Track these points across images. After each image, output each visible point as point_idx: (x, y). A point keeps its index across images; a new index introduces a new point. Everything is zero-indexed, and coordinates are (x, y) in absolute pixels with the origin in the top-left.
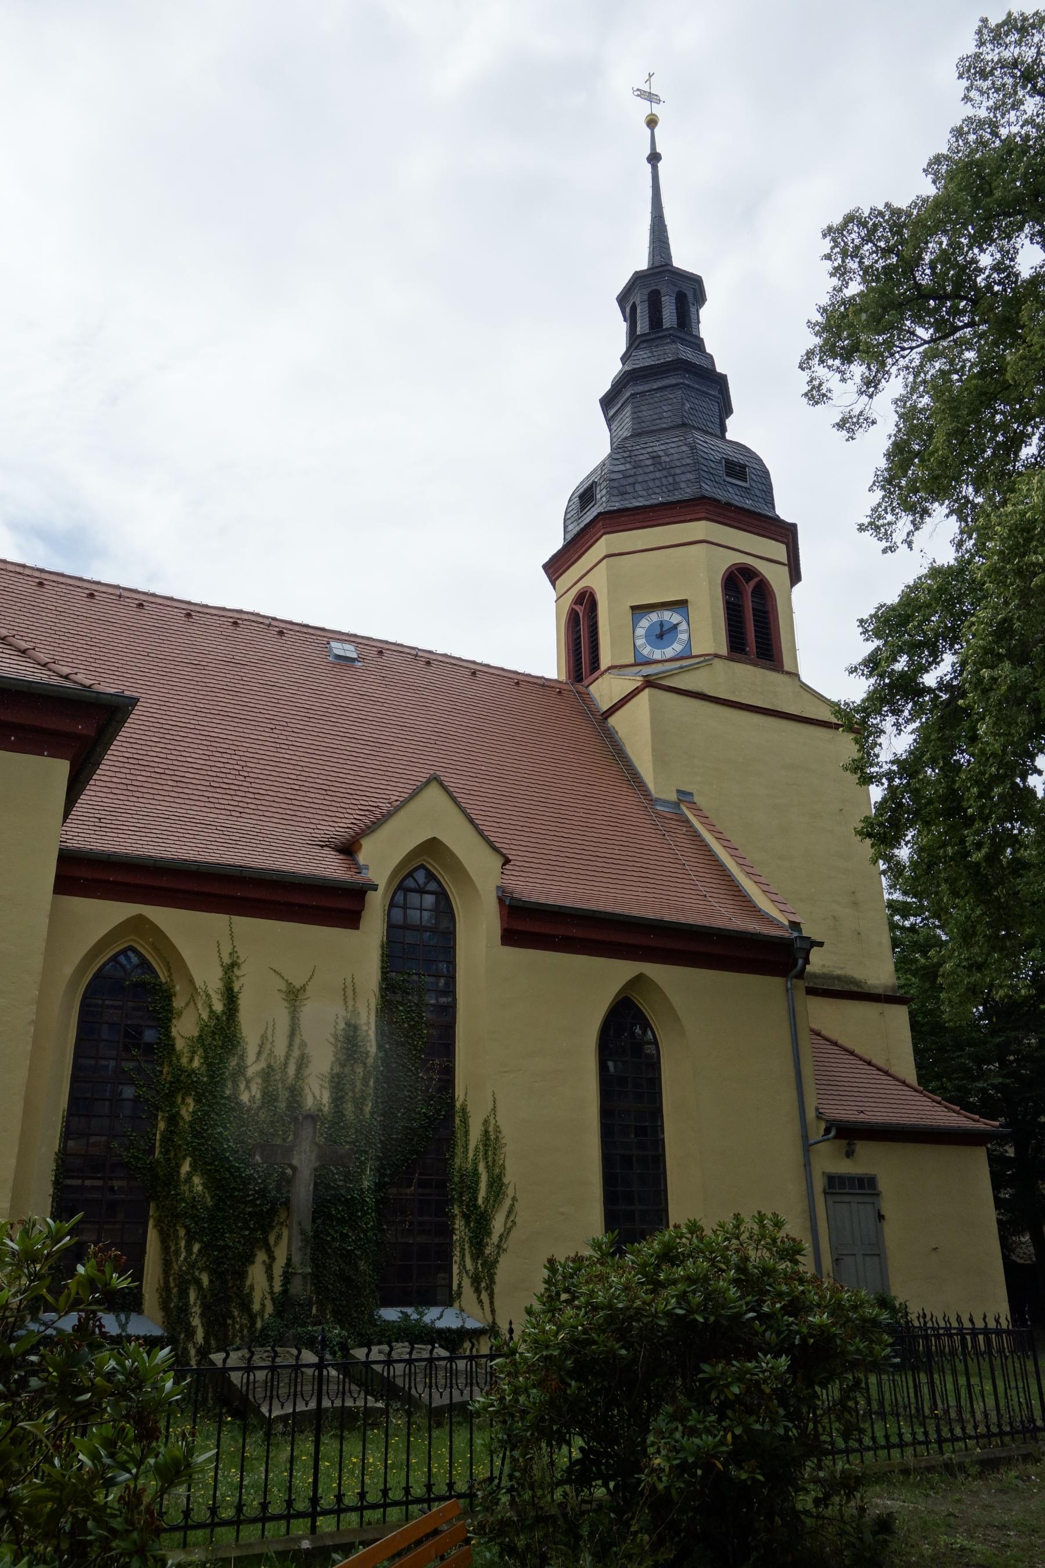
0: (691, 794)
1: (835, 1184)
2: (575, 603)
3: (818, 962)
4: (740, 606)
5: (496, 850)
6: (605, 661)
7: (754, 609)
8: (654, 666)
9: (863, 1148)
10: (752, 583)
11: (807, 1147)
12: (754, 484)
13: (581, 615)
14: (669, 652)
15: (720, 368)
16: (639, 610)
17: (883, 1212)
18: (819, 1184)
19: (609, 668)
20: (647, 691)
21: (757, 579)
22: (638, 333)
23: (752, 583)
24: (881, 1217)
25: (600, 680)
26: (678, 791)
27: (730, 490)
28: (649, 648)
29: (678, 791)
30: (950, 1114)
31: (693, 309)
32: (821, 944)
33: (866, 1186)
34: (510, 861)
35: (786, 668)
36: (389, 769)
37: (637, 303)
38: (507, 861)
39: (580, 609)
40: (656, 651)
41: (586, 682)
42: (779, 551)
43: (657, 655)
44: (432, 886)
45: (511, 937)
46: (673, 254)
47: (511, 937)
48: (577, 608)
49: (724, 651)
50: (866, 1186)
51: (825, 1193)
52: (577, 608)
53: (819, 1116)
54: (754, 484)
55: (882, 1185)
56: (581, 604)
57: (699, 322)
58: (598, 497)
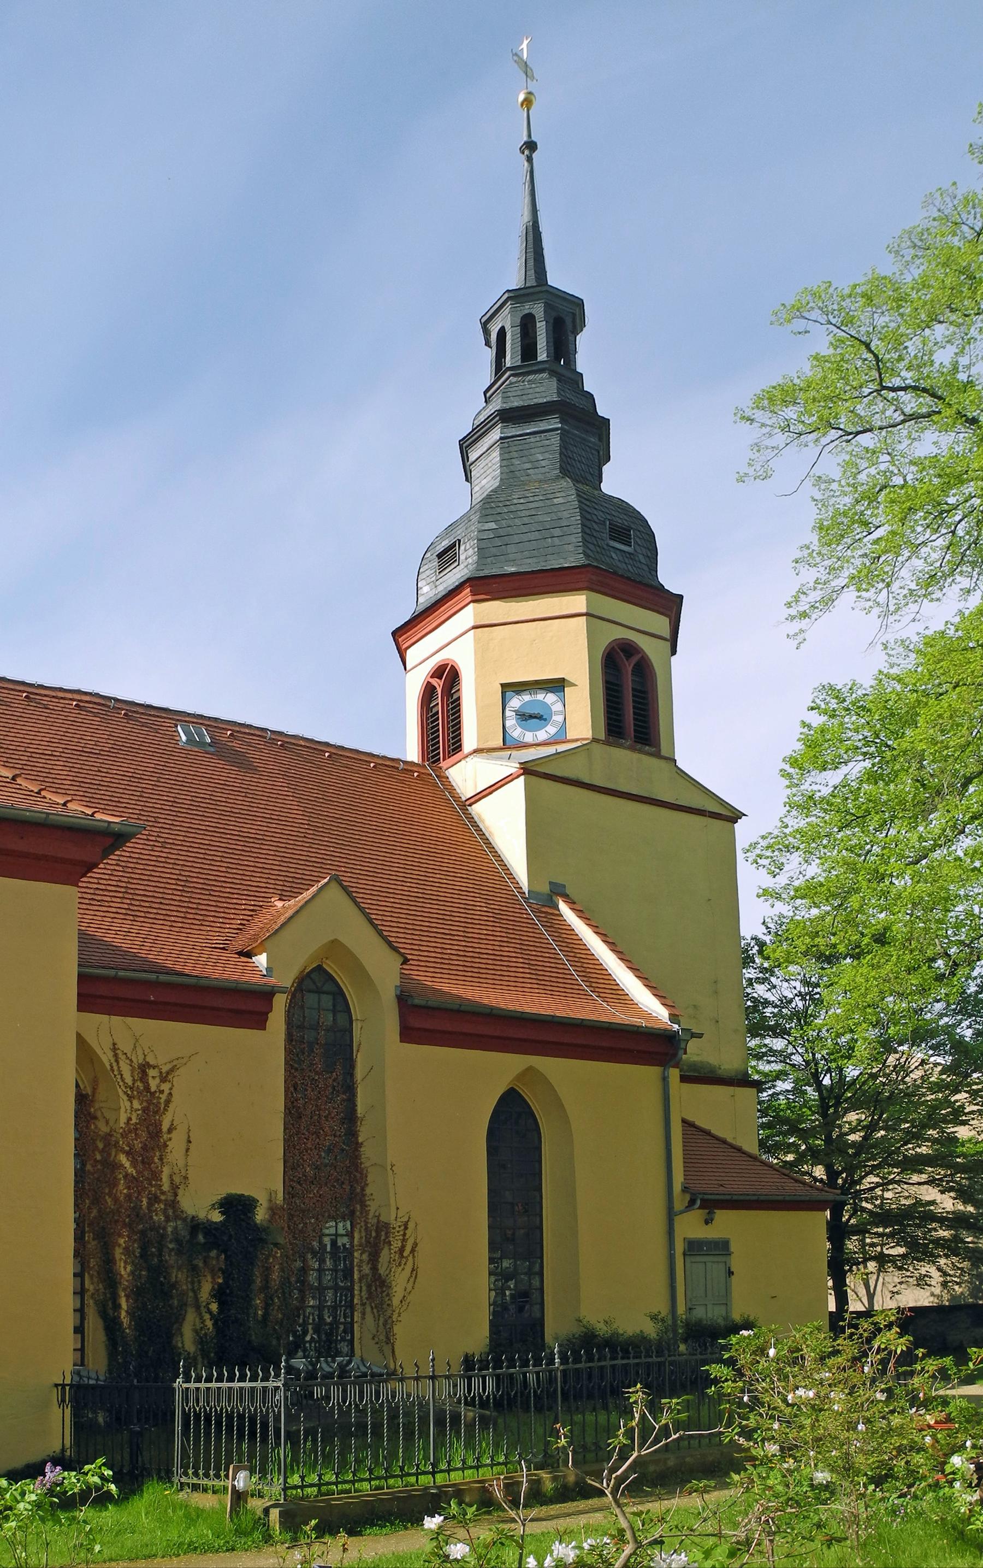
0: (564, 886)
1: (694, 1248)
2: (431, 677)
3: (694, 1052)
4: (644, 692)
5: (395, 949)
6: (470, 740)
7: (633, 689)
8: (524, 751)
9: (721, 1216)
10: (634, 660)
11: (671, 1215)
12: (639, 550)
13: (439, 690)
14: (542, 735)
15: (601, 411)
16: (509, 689)
17: (732, 1270)
18: (679, 1247)
19: (475, 751)
20: (522, 778)
21: (640, 655)
22: (508, 365)
23: (634, 660)
24: (731, 1273)
25: (463, 762)
26: (550, 883)
27: (614, 555)
28: (519, 730)
29: (550, 883)
30: (797, 1185)
31: (571, 338)
32: (700, 1036)
33: (722, 1247)
34: (409, 960)
35: (663, 753)
36: (36, 764)
37: (508, 328)
38: (406, 961)
39: (438, 684)
40: (527, 733)
41: (443, 764)
42: (660, 623)
43: (529, 737)
44: (328, 987)
45: (409, 1034)
46: (548, 268)
47: (409, 1034)
48: (435, 682)
49: (602, 736)
50: (722, 1247)
51: (684, 1254)
52: (435, 682)
53: (685, 1189)
54: (638, 548)
55: (733, 1247)
56: (440, 678)
57: (576, 352)
58: (462, 557)
